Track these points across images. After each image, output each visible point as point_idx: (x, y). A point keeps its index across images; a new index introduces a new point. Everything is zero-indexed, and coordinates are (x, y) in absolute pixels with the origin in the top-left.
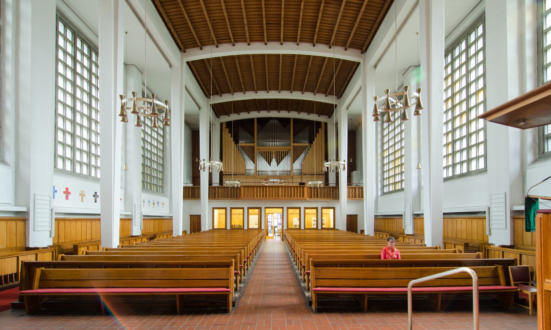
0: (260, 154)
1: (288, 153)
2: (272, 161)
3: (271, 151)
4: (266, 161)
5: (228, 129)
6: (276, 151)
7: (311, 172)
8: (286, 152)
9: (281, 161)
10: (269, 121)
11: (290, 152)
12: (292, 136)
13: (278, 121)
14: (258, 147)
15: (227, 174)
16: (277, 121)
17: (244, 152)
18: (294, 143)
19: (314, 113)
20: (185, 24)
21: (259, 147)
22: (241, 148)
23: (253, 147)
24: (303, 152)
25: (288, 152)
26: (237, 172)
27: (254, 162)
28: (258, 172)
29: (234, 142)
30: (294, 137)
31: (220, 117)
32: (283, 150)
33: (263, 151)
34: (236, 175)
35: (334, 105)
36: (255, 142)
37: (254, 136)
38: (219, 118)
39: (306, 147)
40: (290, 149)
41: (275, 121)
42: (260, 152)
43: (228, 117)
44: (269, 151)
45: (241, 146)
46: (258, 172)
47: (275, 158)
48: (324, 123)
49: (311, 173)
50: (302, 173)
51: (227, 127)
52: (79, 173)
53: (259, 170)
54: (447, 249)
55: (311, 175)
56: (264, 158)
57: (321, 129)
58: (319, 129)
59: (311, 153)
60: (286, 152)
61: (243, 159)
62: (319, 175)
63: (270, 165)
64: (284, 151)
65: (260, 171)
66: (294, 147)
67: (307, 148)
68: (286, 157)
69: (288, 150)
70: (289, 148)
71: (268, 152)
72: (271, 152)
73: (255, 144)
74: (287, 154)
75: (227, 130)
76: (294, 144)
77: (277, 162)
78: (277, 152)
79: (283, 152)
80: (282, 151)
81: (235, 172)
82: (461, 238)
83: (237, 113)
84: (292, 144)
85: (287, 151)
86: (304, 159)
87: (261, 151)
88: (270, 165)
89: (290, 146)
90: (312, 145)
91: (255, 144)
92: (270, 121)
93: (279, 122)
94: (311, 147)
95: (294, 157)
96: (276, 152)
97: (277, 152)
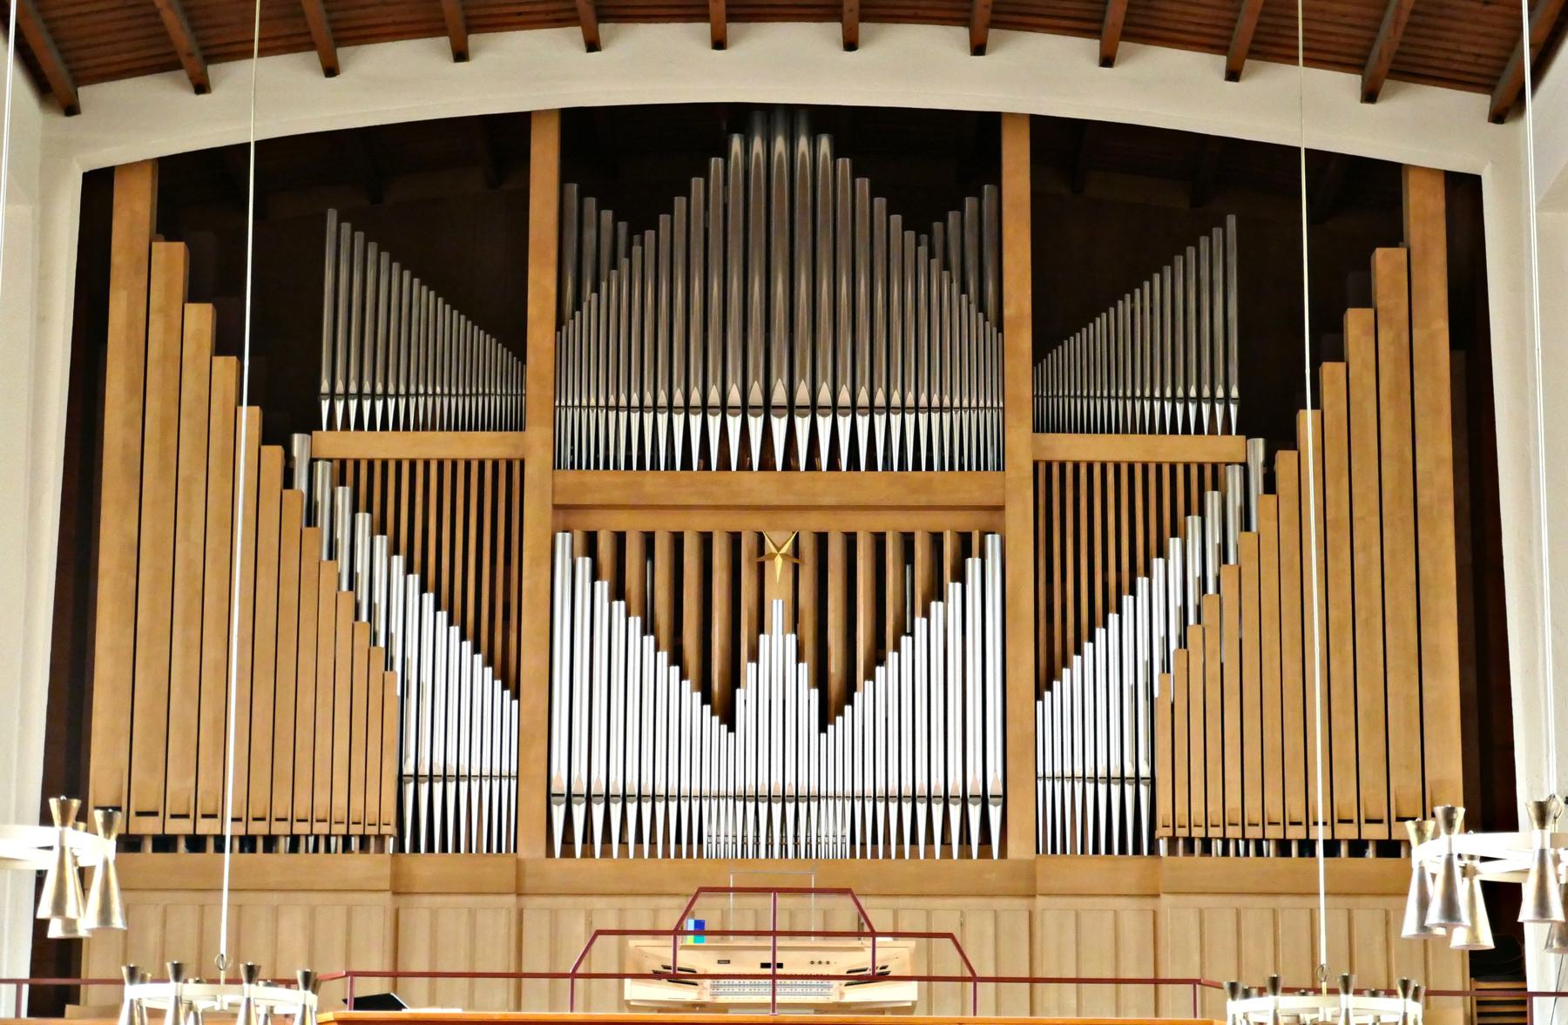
0: (595, 576)
1: (973, 565)
2: (754, 656)
3: (747, 526)
4: (677, 658)
5: (179, 248)
6: (817, 522)
7: (1275, 812)
8: (937, 539)
9: (877, 658)
10: (725, 153)
11: (993, 542)
12: (1020, 339)
13: (837, 153)
14: (569, 477)
15: (181, 827)
16: (825, 145)
17: (381, 542)
18: (1040, 426)
19: (1293, 60)
20: (168, 54)
21: (591, 477)
22: (344, 495)
23: (511, 472)
24: (1162, 552)
25: (965, 547)
26: (281, 809)
27: (510, 679)
28: (559, 813)
29: (256, 409)
30: (1043, 346)
31: (88, 95)
32: (906, 522)
33: (634, 525)
34: (270, 842)
35: (1299, 149)
36: (531, 416)
37: (515, 341)
38: (71, 109)
39: (1213, 476)
40: (1000, 509)
41: (803, 144)
42: (591, 545)
43: (190, 98)
44: (720, 527)
45: (343, 471)
46: (559, 813)
47: (795, 624)
48: (1439, 187)
49: (1274, 833)
50: (1162, 833)
51: (166, 226)
52: (160, 835)
53: (777, 790)
54: (936, 1014)
55: (1283, 847)
56: (648, 627)
57: (1399, 254)
58: (1380, 253)
59: (1269, 558)
60: (937, 539)
61: (362, 639)
62: (164, 843)
63: (728, 718)
64: (920, 525)
65: (797, 799)
66: (1044, 472)
67: (1212, 499)
68: (936, 607)
69: (963, 521)
70: (971, 487)
71: (706, 540)
72: (735, 539)
73: (535, 444)
74: (960, 575)
75: (172, 257)
76: (1049, 439)
77: (820, 679)
78: (822, 539)
79: (907, 540)
80: (891, 525)
81: (302, 810)
82: (777, 938)
83: (308, 46)
84: (1023, 446)
85: (949, 525)
86: (1183, 642)
87: (594, 521)
88: (728, 718)
89: (1000, 467)
90: (1285, 459)
91: (535, 444)
92: (736, 144)
93: (845, 164)
94: (1270, 486)
95: (1045, 614)
96: (808, 546)
97: (822, 539)
